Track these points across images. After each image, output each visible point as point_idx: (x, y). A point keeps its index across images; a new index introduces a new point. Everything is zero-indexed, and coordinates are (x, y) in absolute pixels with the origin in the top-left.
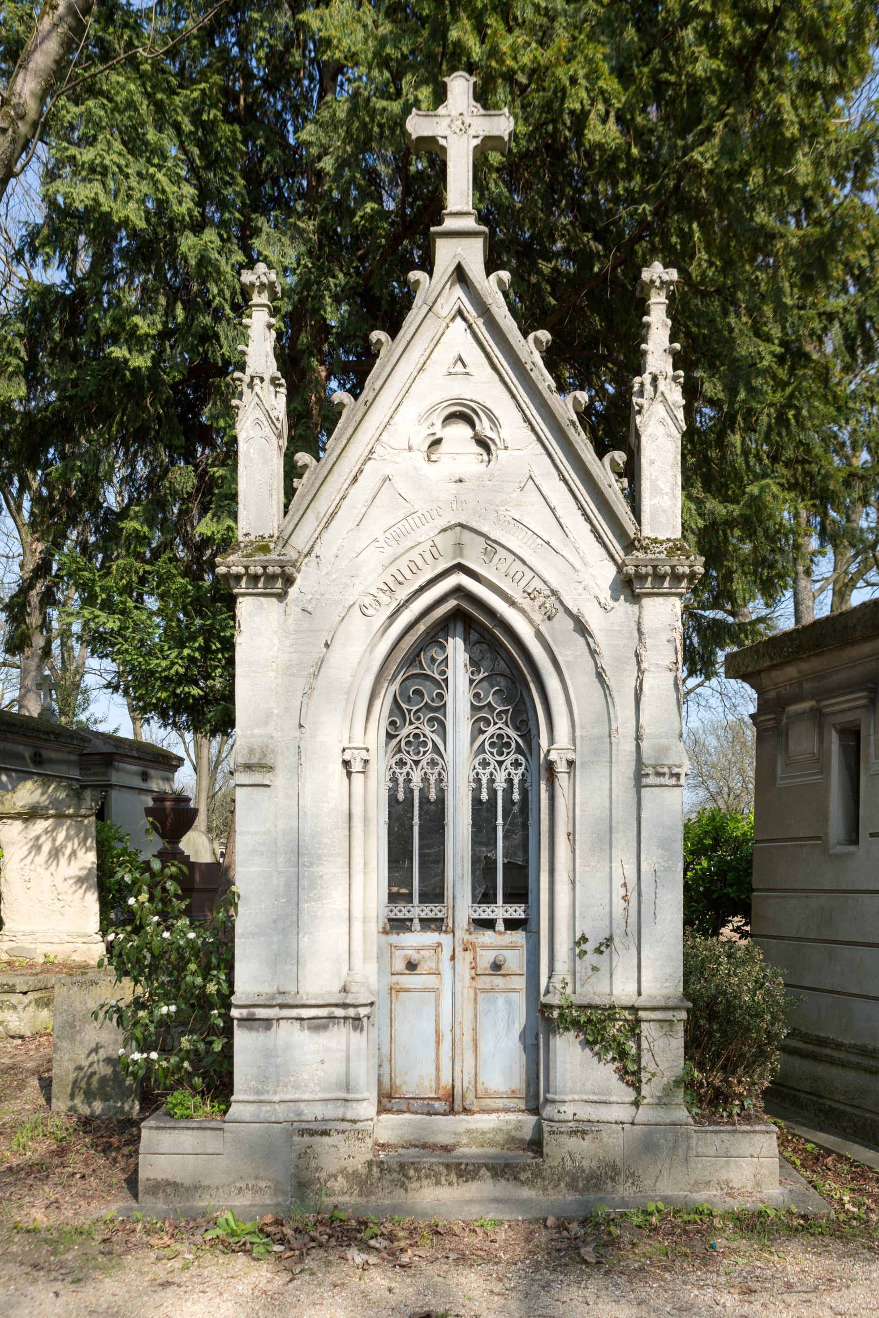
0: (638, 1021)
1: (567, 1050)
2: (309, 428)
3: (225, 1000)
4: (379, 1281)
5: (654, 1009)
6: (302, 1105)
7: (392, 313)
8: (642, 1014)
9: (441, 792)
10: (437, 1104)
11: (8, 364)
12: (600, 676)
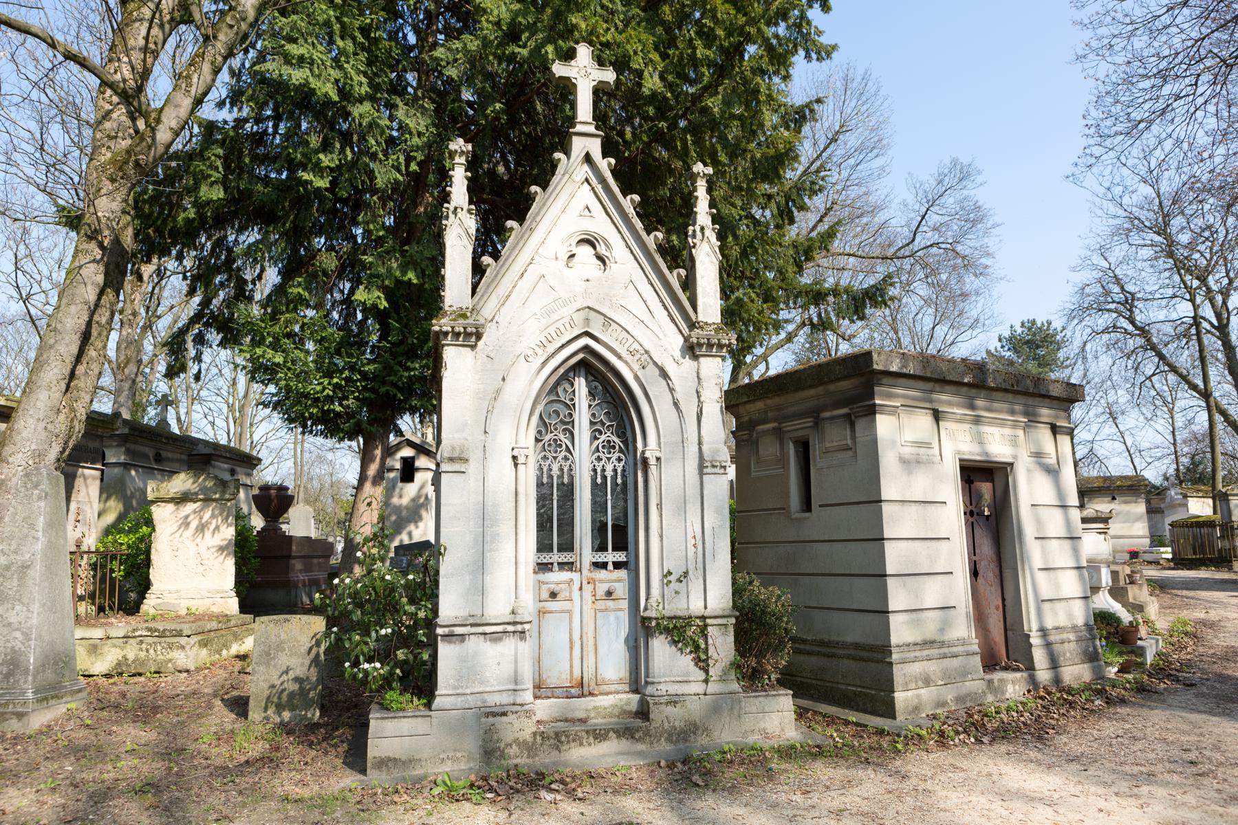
0: (706, 626)
1: (660, 648)
2: (489, 242)
3: (430, 623)
4: (571, 808)
5: (716, 617)
6: (485, 695)
7: (545, 177)
8: (709, 621)
9: (571, 477)
10: (573, 691)
11: (210, 176)
12: (676, 404)
